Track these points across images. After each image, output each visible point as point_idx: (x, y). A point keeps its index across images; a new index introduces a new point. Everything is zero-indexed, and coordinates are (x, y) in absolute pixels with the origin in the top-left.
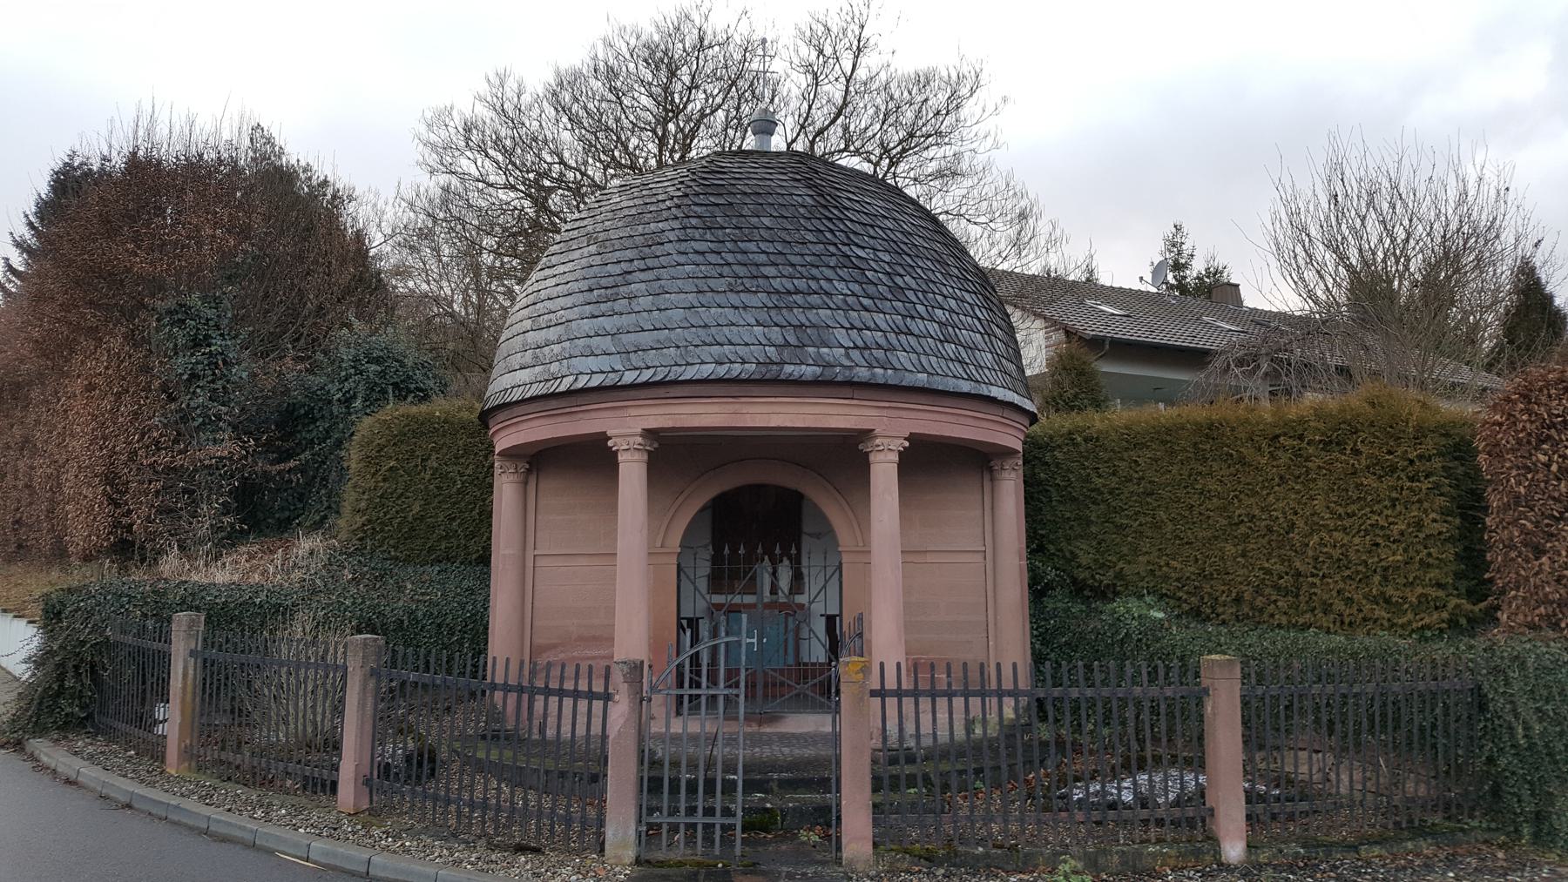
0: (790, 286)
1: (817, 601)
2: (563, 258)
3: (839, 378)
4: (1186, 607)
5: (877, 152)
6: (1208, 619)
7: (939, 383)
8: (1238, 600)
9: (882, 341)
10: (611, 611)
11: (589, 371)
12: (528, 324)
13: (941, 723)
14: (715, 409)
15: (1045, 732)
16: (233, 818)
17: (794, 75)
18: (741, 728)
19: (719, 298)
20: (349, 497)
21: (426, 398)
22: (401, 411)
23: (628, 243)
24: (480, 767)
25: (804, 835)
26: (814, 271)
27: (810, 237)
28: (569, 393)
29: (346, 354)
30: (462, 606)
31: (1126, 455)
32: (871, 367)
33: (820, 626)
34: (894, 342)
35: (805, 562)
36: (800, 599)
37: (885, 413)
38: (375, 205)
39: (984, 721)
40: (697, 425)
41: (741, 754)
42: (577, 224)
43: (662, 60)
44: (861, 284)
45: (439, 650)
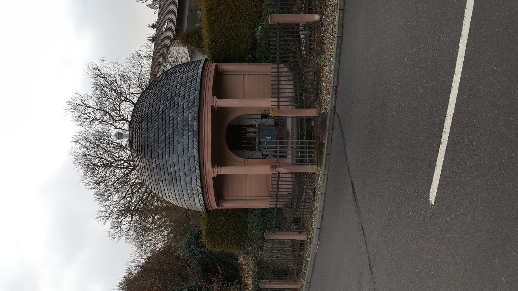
0: (172, 128)
1: (258, 120)
2: (163, 191)
3: (198, 115)
4: (258, 20)
5: (119, 100)
6: (261, 14)
7: (198, 87)
8: (256, 6)
9: (187, 103)
10: (260, 175)
11: (196, 183)
12: (182, 200)
13: (288, 88)
14: (206, 149)
15: (291, 60)
16: (309, 265)
17: (93, 126)
18: (290, 140)
19: (176, 148)
20: (229, 250)
21: (200, 231)
22: (204, 237)
23: (159, 173)
24: (298, 207)
25: (313, 125)
26: (167, 122)
27: (157, 123)
28: (202, 188)
29: (188, 254)
30: (258, 217)
31: (216, 34)
32: (194, 106)
33: (264, 120)
34: (187, 100)
35: (247, 124)
36: (257, 125)
37: (207, 103)
38: (132, 262)
39: (288, 76)
40: (463, 28)
41: (295, 140)
42: (153, 188)
43: (91, 168)
44: (170, 109)
45: (270, 219)
